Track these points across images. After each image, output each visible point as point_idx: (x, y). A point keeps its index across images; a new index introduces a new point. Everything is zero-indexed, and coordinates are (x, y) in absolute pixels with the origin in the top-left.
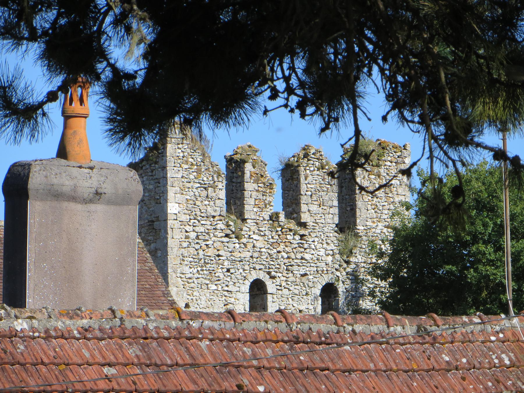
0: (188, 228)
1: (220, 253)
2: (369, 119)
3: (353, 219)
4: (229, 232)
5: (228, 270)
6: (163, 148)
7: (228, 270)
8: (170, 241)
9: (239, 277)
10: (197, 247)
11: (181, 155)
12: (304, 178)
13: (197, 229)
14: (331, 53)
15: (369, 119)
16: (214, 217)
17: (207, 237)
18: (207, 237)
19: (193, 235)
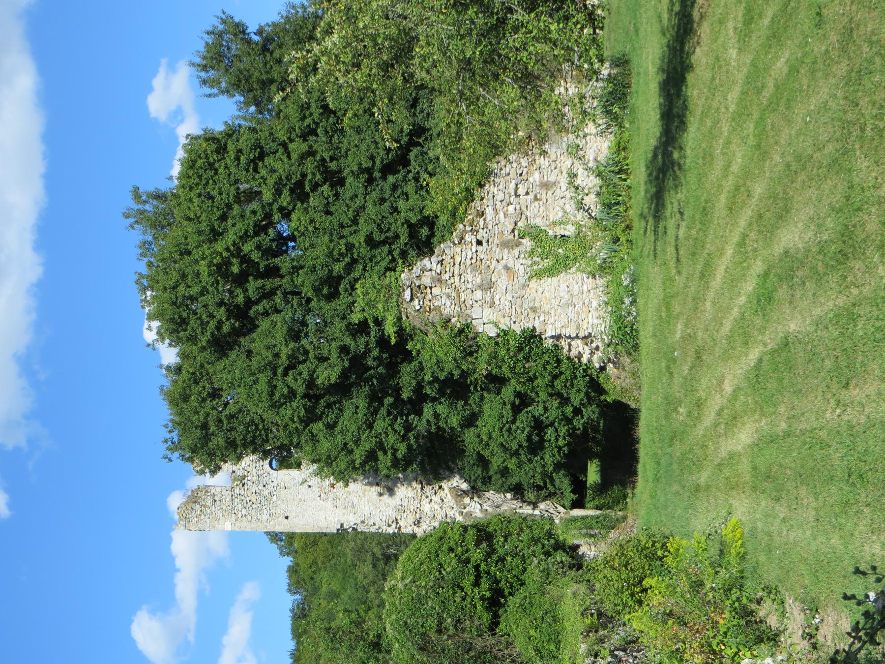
0: (240, 516)
1: (254, 492)
2: (846, 597)
3: (323, 544)
4: (241, 484)
5: (264, 486)
6: (232, 445)
7: (264, 486)
8: (248, 530)
9: (268, 478)
10: (251, 508)
11: (196, 519)
12: (669, 232)
13: (240, 509)
14: (572, 405)
15: (846, 597)
16: (232, 495)
17: (244, 501)
18: (244, 501)
19: (244, 512)
